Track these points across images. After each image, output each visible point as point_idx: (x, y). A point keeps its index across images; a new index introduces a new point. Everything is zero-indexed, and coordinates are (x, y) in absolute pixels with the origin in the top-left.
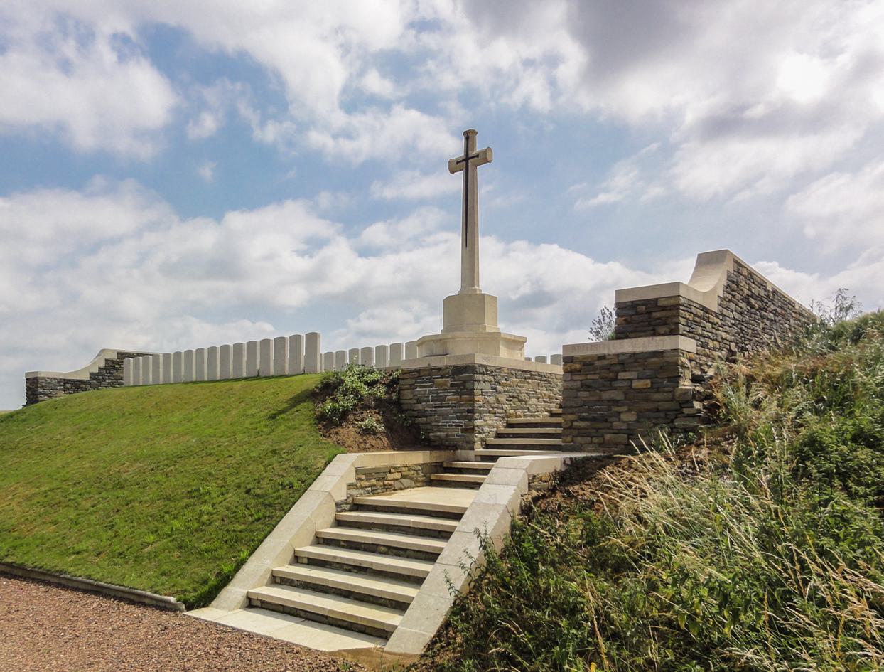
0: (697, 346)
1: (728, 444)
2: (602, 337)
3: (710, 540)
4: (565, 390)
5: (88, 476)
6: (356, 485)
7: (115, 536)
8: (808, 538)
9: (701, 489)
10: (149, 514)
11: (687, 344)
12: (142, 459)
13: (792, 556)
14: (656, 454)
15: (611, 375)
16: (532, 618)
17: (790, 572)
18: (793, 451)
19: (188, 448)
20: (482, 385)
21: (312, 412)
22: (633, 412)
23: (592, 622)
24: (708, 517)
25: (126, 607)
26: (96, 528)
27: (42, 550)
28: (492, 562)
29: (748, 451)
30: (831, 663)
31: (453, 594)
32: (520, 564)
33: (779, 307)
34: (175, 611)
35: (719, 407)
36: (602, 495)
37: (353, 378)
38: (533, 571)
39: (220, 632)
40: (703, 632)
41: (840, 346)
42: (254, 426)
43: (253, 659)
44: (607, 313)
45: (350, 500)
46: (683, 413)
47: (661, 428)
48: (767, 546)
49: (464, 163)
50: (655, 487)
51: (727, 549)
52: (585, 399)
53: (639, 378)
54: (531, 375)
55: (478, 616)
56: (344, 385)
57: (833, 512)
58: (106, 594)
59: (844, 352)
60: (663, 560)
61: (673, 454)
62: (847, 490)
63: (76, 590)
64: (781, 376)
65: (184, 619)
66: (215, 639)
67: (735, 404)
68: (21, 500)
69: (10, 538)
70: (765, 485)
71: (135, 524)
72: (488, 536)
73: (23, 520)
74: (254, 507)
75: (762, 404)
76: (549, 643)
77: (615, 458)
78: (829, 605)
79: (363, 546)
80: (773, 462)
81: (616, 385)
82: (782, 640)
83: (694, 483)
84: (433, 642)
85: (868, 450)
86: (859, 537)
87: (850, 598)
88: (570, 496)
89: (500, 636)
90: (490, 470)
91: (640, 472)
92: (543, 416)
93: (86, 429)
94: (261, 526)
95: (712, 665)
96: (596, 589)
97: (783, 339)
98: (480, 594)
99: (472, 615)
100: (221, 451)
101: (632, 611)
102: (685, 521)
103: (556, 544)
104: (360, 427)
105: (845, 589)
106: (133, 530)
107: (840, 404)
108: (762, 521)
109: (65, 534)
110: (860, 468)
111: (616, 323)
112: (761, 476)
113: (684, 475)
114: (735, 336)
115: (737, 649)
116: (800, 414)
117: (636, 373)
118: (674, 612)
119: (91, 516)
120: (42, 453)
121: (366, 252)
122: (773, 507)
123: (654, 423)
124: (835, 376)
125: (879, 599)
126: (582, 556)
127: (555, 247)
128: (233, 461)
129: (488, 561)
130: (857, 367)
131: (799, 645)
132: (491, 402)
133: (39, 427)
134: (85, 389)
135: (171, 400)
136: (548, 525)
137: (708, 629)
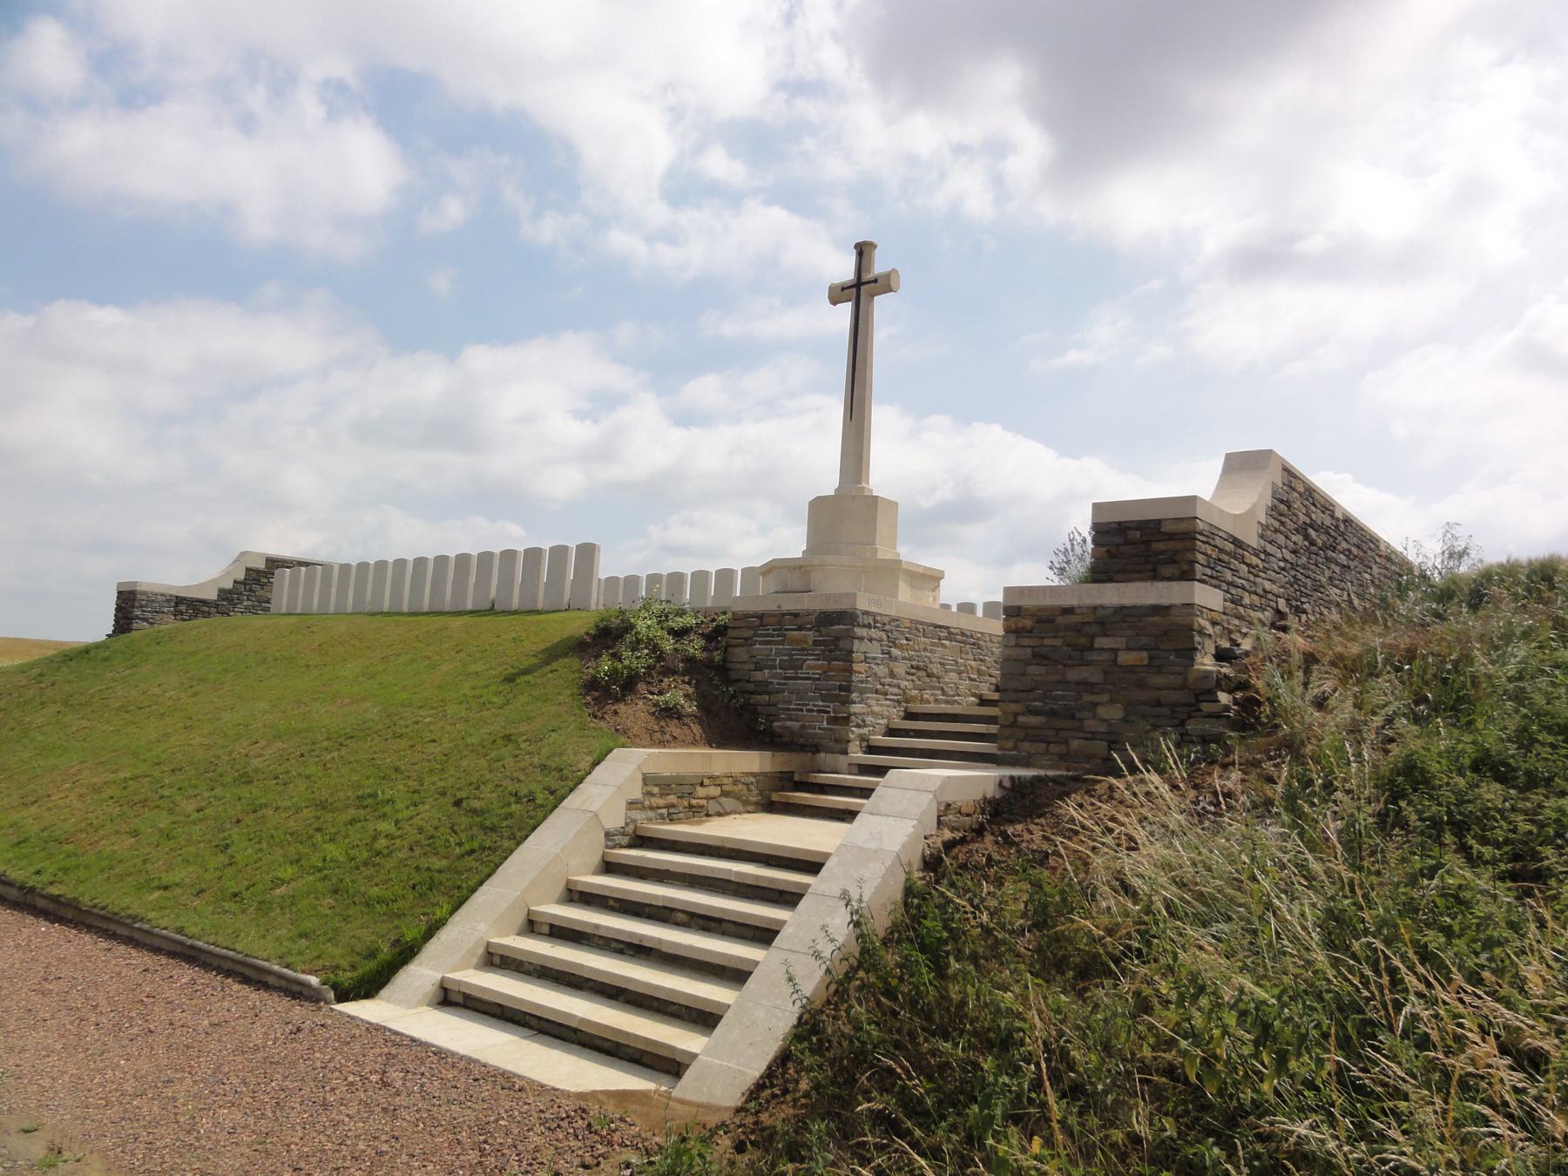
0: (1225, 600)
1: (1275, 766)
2: (1069, 578)
3: (1242, 929)
4: (1006, 661)
5: (195, 760)
6: (642, 803)
7: (230, 864)
8: (1403, 931)
9: (1228, 840)
10: (290, 831)
11: (1208, 597)
12: (287, 737)
13: (1377, 962)
14: (1154, 778)
15: (1083, 641)
16: (934, 1052)
17: (1373, 988)
18: (1379, 782)
19: (364, 722)
20: (865, 646)
21: (577, 675)
22: (1118, 705)
23: (1038, 1065)
24: (1239, 889)
25: (236, 987)
26: (199, 848)
27: (108, 878)
28: (869, 951)
29: (1306, 779)
30: (1437, 1147)
31: (798, 1004)
32: (917, 956)
33: (1354, 545)
34: (317, 1001)
35: (1259, 704)
36: (1062, 842)
37: (649, 622)
38: (940, 969)
39: (389, 1044)
40: (1226, 1089)
41: (1452, 614)
42: (477, 692)
43: (443, 1096)
44: (1079, 539)
45: (630, 829)
46: (1200, 710)
47: (1165, 734)
48: (1337, 942)
49: (854, 290)
50: (1152, 834)
51: (1270, 944)
52: (1038, 678)
53: (1128, 649)
54: (950, 633)
55: (840, 1043)
56: (633, 633)
57: (1443, 888)
58: (204, 962)
59: (1457, 623)
60: (1163, 961)
61: (1183, 778)
62: (1465, 851)
63: (156, 950)
64: (1360, 657)
65: (331, 1017)
66: (380, 1055)
67: (1286, 700)
68: (85, 791)
69: (60, 854)
70: (1334, 838)
71: (264, 845)
72: (864, 905)
73: (84, 824)
74: (465, 830)
75: (1330, 702)
76: (962, 1098)
77: (1086, 781)
78: (1435, 1047)
79: (647, 910)
80: (1346, 799)
81: (1090, 658)
82: (1358, 1105)
83: (1218, 829)
84: (759, 1087)
85: (1498, 786)
86: (1485, 931)
87: (1469, 1034)
88: (1008, 841)
89: (877, 1082)
90: (873, 790)
91: (1128, 807)
92: (965, 703)
93: (201, 680)
94: (474, 864)
95: (1240, 1147)
96: (1047, 1005)
97: (1361, 597)
98: (845, 1005)
99: (829, 1042)
100: (418, 731)
101: (1107, 1048)
102: (1202, 894)
103: (981, 925)
104: (656, 705)
105: (1461, 1020)
106: (260, 855)
107: (1452, 708)
108: (1328, 899)
109: (147, 854)
110: (1485, 815)
111: (1093, 556)
112: (1327, 822)
113: (1201, 816)
114: (1286, 588)
115: (1283, 1119)
116: (1389, 721)
117: (1124, 640)
118: (1179, 1051)
119: (194, 828)
120: (127, 716)
121: (684, 418)
122: (1347, 875)
123: (1152, 725)
124: (1443, 662)
125: (1516, 1038)
126: (1025, 948)
127: (996, 428)
128: (439, 749)
129: (863, 948)
130: (1478, 650)
131: (1387, 1115)
132: (880, 674)
133: (129, 671)
134: (208, 615)
135: (346, 641)
136: (969, 890)
137: (1235, 1084)
